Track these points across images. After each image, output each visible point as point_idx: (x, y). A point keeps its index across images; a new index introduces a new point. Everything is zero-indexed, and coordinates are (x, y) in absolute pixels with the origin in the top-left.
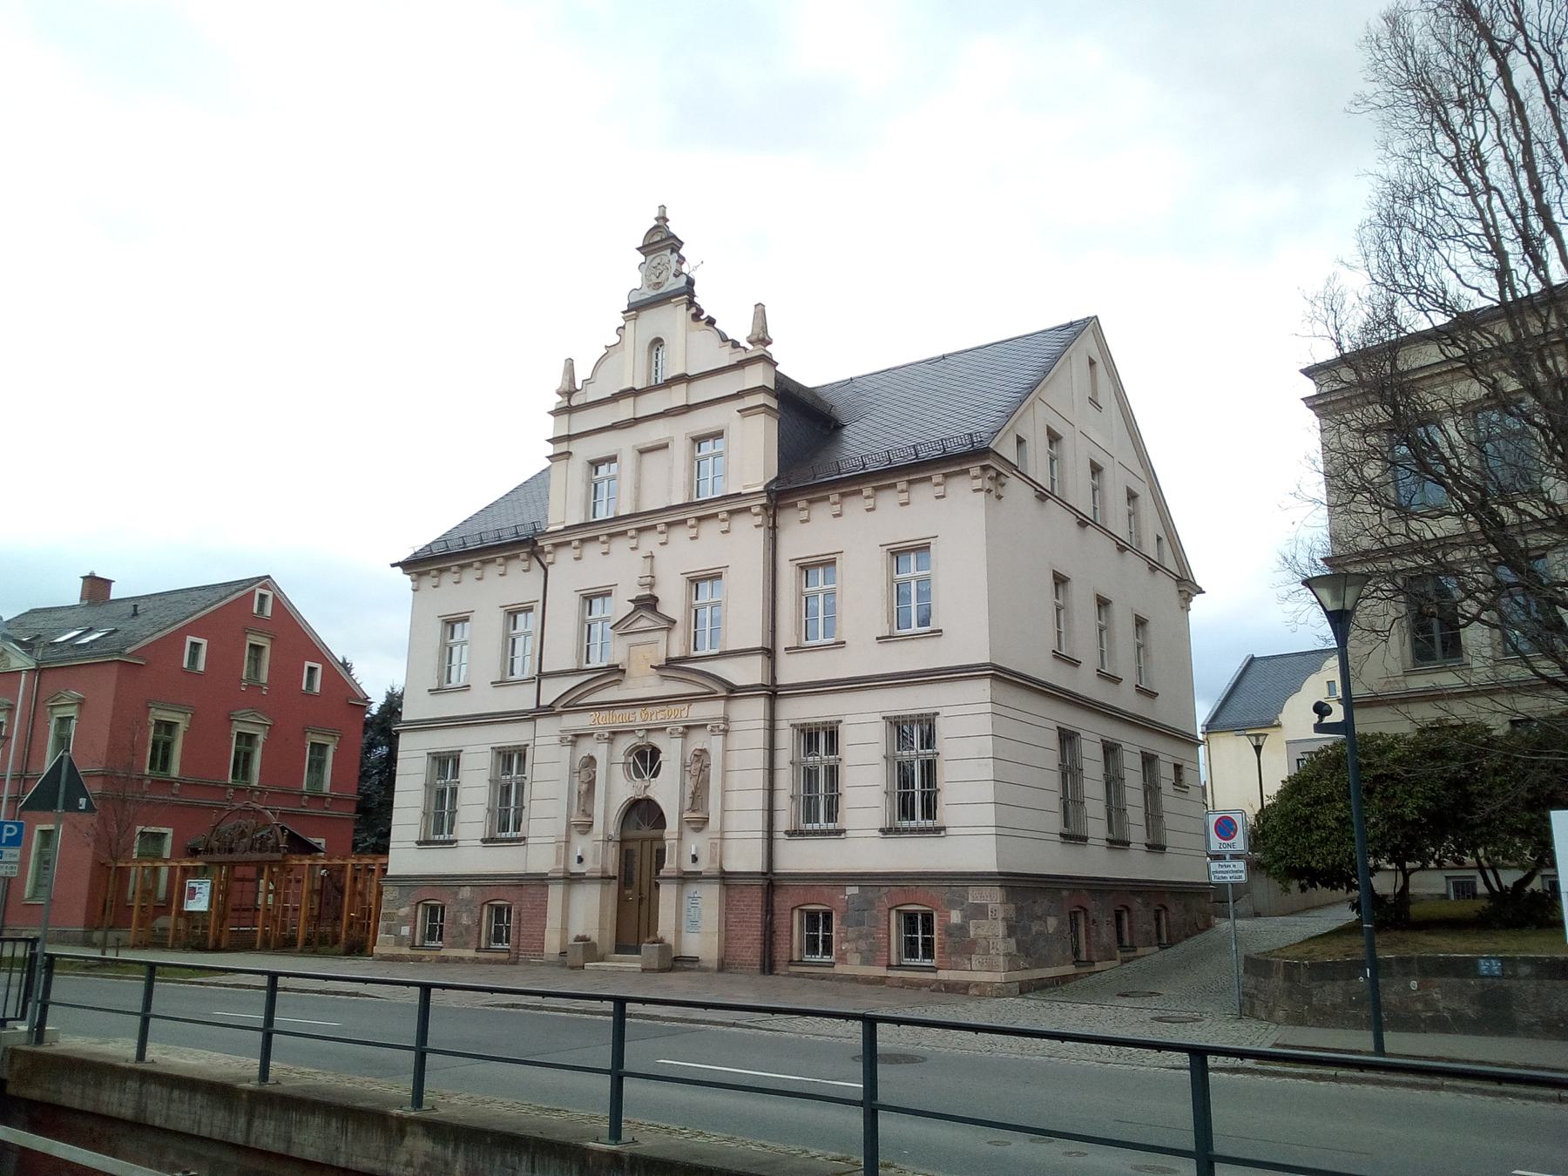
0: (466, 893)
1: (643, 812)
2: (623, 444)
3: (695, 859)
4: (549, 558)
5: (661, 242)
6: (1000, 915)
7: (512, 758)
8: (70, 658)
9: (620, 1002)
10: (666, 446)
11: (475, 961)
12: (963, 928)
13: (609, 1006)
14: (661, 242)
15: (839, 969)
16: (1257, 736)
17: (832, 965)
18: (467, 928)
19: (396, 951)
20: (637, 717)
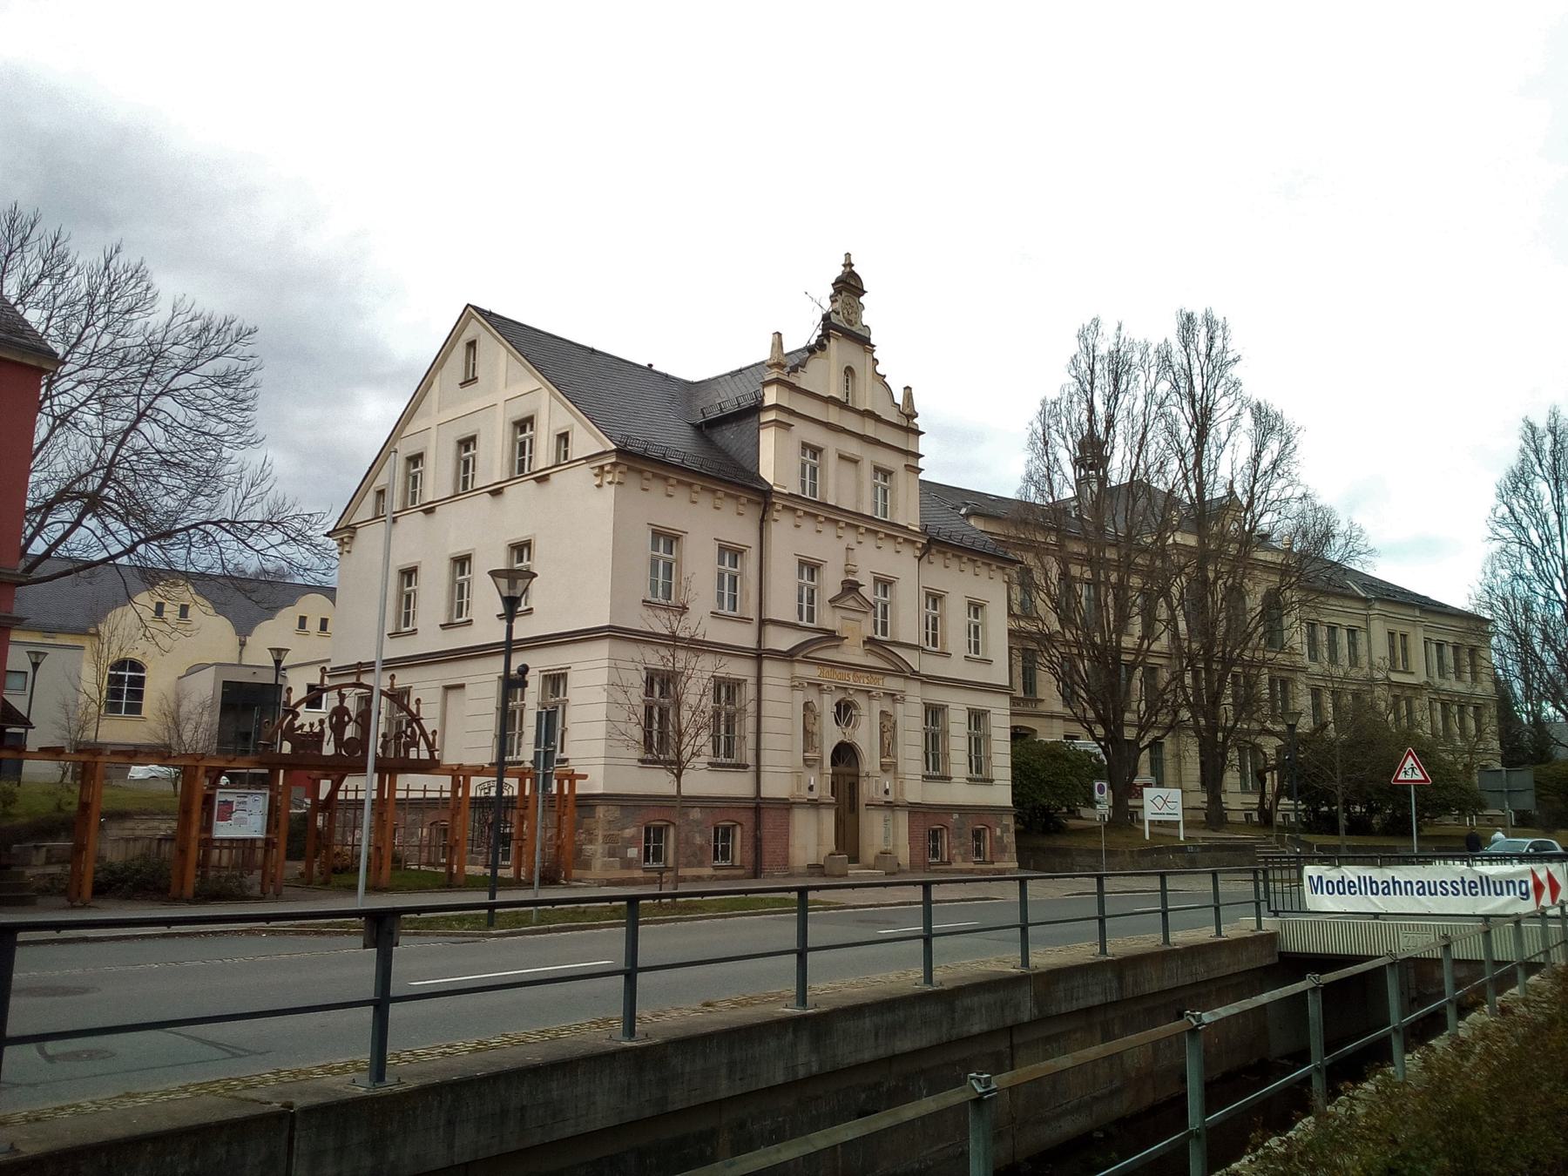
0: (696, 814)
1: (845, 754)
5: (849, 286)
6: (1012, 830)
7: (556, 681)
8: (328, 925)
9: (803, 891)
10: (856, 462)
12: (1001, 838)
13: (794, 895)
14: (849, 286)
15: (954, 866)
16: (37, 653)
17: (949, 863)
18: (701, 847)
19: (626, 874)
20: (851, 679)
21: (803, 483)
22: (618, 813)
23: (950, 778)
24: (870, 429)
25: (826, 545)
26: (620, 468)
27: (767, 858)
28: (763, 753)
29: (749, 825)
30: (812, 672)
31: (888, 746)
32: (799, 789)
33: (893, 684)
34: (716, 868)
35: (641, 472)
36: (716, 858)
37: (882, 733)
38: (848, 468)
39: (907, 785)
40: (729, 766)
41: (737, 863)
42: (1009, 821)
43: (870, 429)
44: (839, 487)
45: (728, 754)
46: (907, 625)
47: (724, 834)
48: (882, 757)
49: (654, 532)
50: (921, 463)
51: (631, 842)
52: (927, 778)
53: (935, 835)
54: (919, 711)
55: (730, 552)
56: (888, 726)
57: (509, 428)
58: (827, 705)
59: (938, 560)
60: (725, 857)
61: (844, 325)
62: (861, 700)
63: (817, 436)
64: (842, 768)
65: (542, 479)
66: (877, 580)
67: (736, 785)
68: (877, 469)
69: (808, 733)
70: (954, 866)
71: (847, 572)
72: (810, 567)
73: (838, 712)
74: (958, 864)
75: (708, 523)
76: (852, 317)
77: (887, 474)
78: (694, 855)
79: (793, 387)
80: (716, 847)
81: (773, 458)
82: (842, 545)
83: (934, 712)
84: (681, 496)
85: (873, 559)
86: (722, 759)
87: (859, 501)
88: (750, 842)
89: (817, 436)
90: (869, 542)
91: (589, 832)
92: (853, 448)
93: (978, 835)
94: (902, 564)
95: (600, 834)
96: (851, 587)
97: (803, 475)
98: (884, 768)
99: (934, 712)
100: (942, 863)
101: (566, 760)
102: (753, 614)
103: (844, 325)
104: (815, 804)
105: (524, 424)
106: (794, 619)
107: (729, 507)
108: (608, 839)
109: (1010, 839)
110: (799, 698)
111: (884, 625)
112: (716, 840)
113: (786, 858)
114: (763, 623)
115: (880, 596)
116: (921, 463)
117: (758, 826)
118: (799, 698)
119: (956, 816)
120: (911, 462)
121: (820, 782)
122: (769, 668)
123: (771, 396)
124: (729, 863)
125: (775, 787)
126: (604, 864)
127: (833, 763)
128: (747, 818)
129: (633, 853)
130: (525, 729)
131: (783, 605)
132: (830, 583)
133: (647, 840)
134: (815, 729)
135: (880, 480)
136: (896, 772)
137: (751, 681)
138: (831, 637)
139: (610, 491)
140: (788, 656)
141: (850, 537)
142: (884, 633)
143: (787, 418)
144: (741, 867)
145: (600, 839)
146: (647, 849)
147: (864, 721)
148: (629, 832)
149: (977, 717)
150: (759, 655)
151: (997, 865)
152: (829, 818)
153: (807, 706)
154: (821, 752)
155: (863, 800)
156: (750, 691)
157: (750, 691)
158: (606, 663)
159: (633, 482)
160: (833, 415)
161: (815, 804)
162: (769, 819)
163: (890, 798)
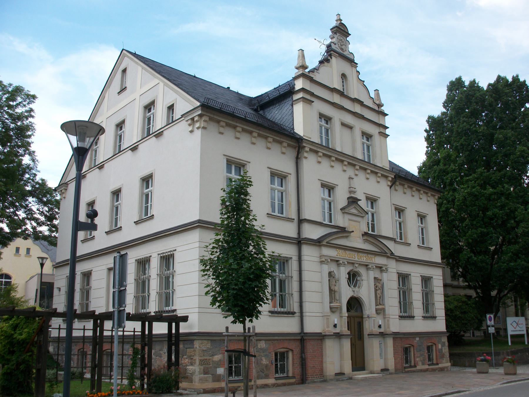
1: (354, 304)
2: (337, 116)
3: (380, 326)
4: (306, 155)
5: (341, 30)
7: (167, 259)
11: (274, 385)
12: (441, 349)
14: (341, 30)
15: (418, 368)
17: (415, 366)
18: (266, 366)
19: (216, 385)
20: (355, 257)
21: (321, 137)
22: (209, 345)
23: (413, 317)
24: (357, 109)
25: (337, 175)
26: (204, 118)
27: (310, 371)
28: (304, 304)
29: (297, 350)
30: (332, 253)
31: (379, 300)
32: (328, 327)
33: (380, 261)
34: (276, 379)
35: (218, 122)
36: (277, 372)
37: (376, 290)
38: (346, 131)
39: (391, 321)
40: (283, 313)
41: (290, 374)
42: (445, 340)
43: (357, 109)
44: (343, 142)
45: (282, 305)
46: (387, 226)
47: (280, 358)
48: (376, 305)
49: (228, 161)
50: (387, 132)
51: (219, 364)
52: (401, 317)
53: (406, 351)
54: (395, 277)
55: (278, 176)
56: (379, 287)
57: (142, 110)
58: (343, 273)
59: (400, 188)
60: (283, 371)
61: (338, 50)
62: (362, 271)
63: (328, 111)
64: (353, 313)
65: (159, 135)
66: (368, 198)
67: (287, 325)
68: (364, 134)
69: (332, 292)
70: (418, 368)
71: (350, 192)
72: (329, 188)
73: (349, 279)
74: (420, 367)
75: (262, 160)
76: (343, 47)
77: (368, 136)
78: (262, 371)
79: (312, 80)
80: (276, 365)
81: (301, 119)
82: (346, 176)
83: (404, 278)
84: (245, 139)
85: (365, 186)
86: (278, 309)
87: (354, 149)
88: (298, 361)
89: (328, 111)
90: (362, 175)
91: (190, 357)
92: (349, 119)
93: (429, 348)
94: (380, 189)
95: (197, 359)
96: (353, 201)
97: (321, 133)
98: (378, 312)
99: (404, 278)
100: (411, 367)
101: (175, 310)
102: (294, 216)
103: (338, 50)
104: (338, 336)
105: (149, 107)
106: (319, 219)
107: (276, 148)
108: (202, 362)
109: (446, 350)
110: (326, 269)
111: (373, 225)
112: (276, 360)
113: (322, 370)
114: (301, 221)
115: (369, 208)
116: (387, 132)
117: (303, 351)
118: (326, 269)
119: (417, 339)
120: (382, 130)
121: (340, 321)
122: (306, 250)
123: (299, 84)
124: (285, 375)
125: (313, 326)
126: (201, 379)
127: (348, 310)
128: (295, 346)
129: (221, 371)
130: (151, 292)
131: (313, 209)
132: (341, 198)
133: (230, 362)
134: (336, 288)
135: (365, 140)
136: (384, 314)
137: (295, 258)
138: (343, 231)
139: (198, 133)
140: (318, 243)
141: (350, 171)
142: (373, 230)
143: (310, 97)
144: (293, 377)
145: (197, 362)
146: (230, 368)
147: (365, 284)
148: (217, 358)
149: (426, 281)
150: (299, 242)
151: (440, 366)
152: (347, 344)
153: (330, 274)
154: (340, 303)
155: (366, 332)
156: (294, 265)
157: (294, 265)
158: (197, 245)
159: (213, 127)
160: (336, 99)
161: (338, 336)
162: (310, 347)
163: (382, 330)
